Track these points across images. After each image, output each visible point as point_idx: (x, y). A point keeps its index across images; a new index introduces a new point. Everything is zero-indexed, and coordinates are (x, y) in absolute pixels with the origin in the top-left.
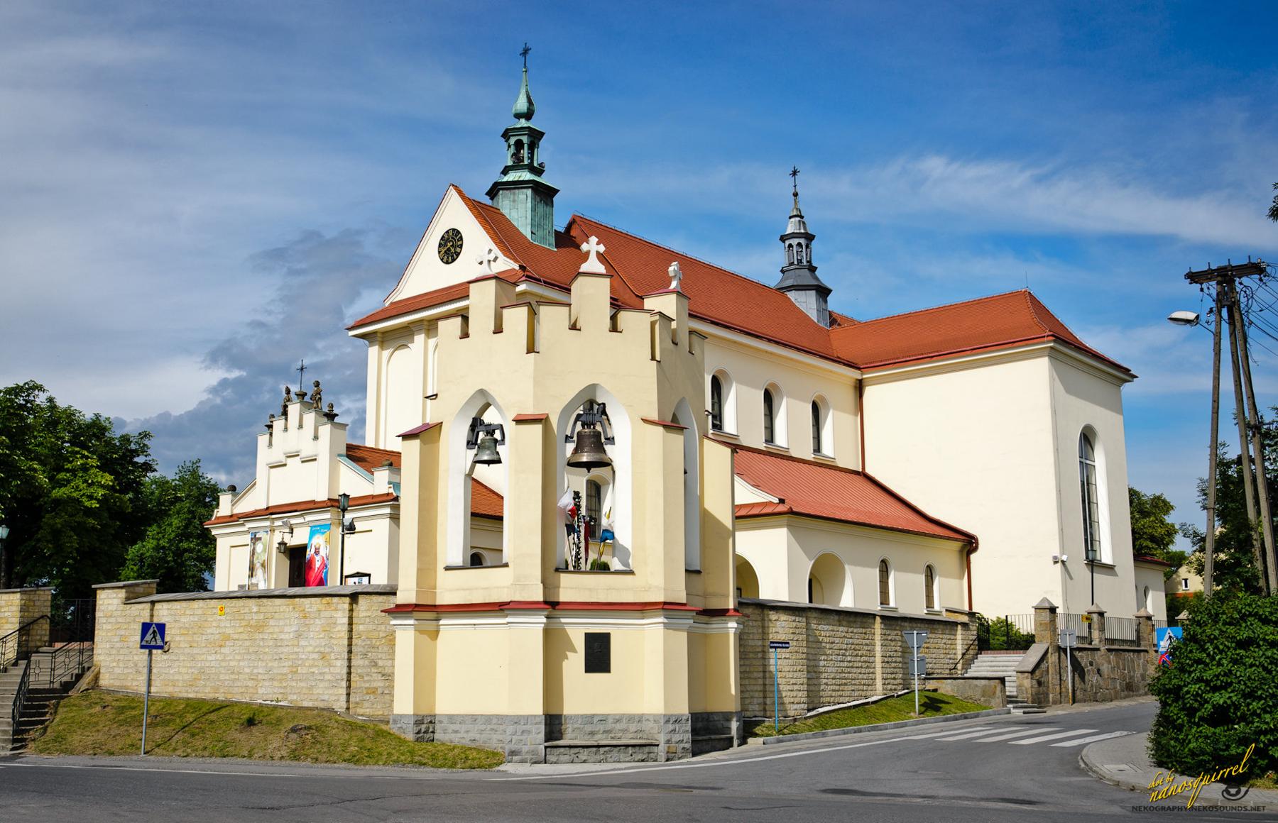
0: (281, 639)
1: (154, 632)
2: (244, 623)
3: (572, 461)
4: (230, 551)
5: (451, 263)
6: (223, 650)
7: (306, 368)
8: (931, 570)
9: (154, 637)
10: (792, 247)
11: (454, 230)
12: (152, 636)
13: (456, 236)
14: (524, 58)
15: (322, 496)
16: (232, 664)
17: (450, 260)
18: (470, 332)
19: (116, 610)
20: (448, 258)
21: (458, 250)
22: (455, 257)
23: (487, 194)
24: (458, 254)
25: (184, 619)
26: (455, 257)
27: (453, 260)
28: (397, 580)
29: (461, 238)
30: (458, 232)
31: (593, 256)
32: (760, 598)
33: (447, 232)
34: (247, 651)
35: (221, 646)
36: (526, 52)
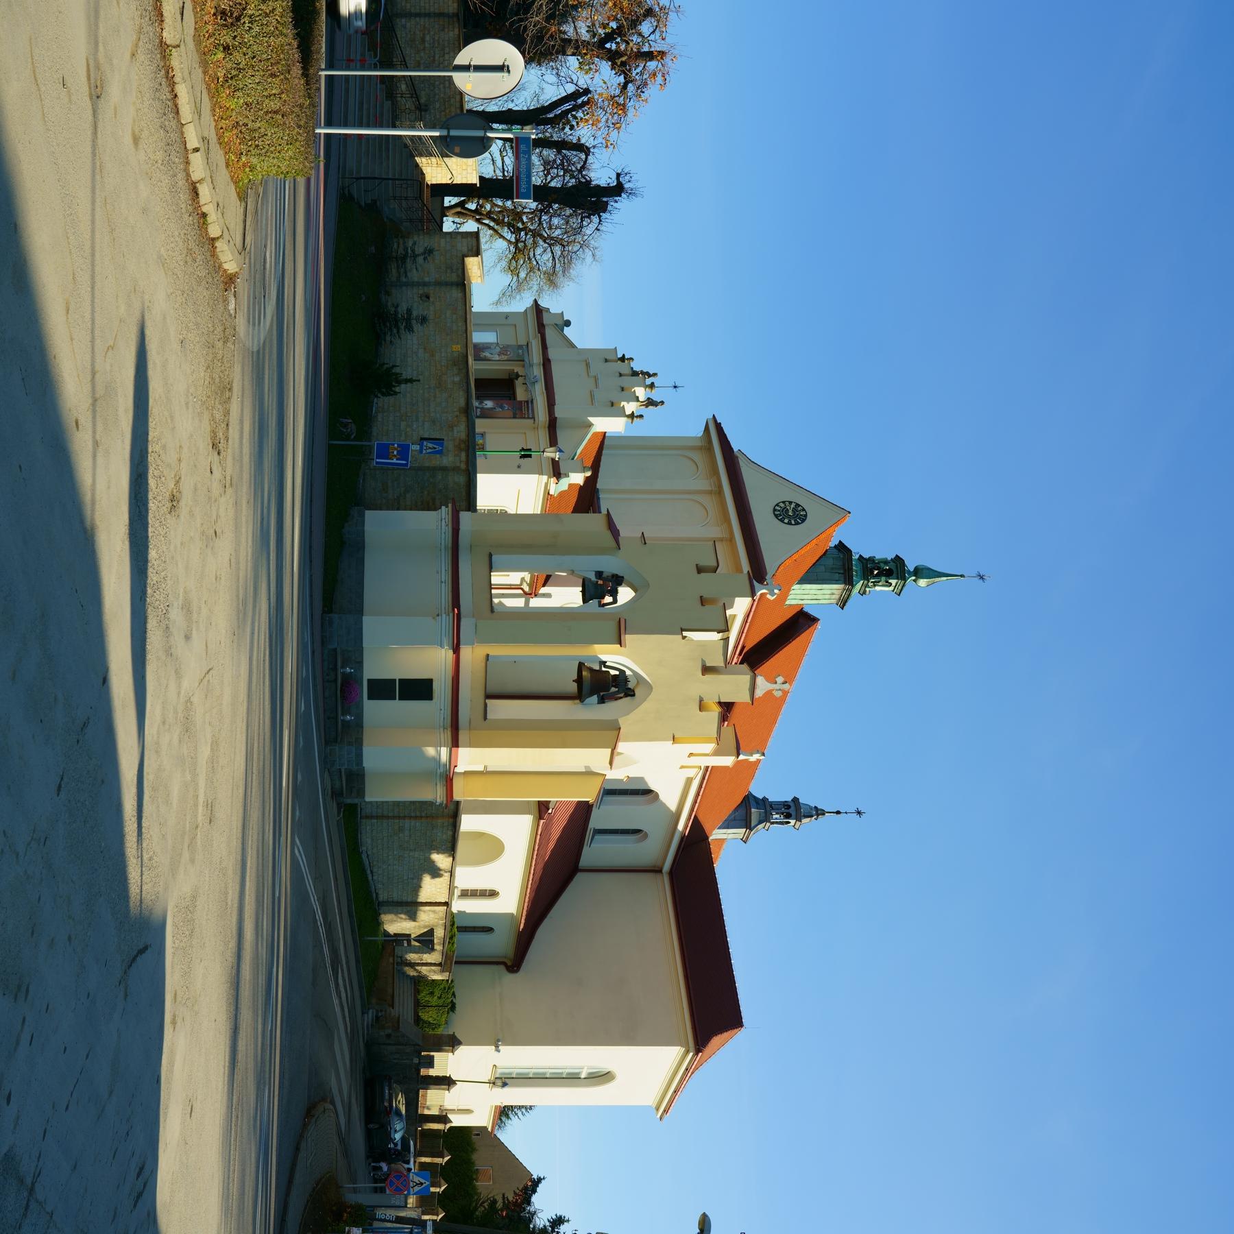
0: (429, 405)
1: (422, 1184)
2: (446, 44)
3: (583, 667)
4: (512, 325)
5: (774, 513)
6: (421, 351)
7: (676, 391)
8: (488, 931)
9: (417, 1184)
10: (788, 809)
11: (806, 516)
12: (418, 1182)
13: (800, 518)
14: (975, 575)
15: (559, 413)
16: (409, 359)
17: (777, 513)
18: (702, 574)
19: (457, 250)
20: (779, 511)
21: (786, 521)
22: (780, 518)
23: (840, 542)
24: (782, 521)
25: (449, 313)
26: (780, 518)
27: (776, 516)
28: (465, 1045)
29: (797, 523)
30: (803, 521)
31: (770, 686)
32: (463, 816)
33: (804, 510)
34: (420, 373)
35: (425, 349)
36: (981, 577)
